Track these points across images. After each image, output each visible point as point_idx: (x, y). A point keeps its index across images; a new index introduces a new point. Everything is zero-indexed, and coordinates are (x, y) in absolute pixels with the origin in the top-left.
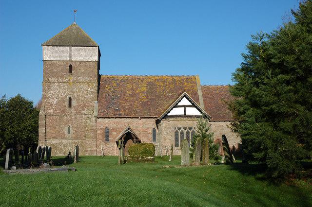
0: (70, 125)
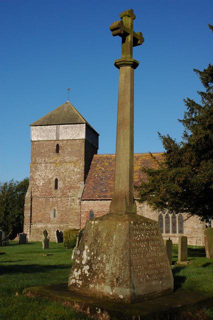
0: (56, 208)
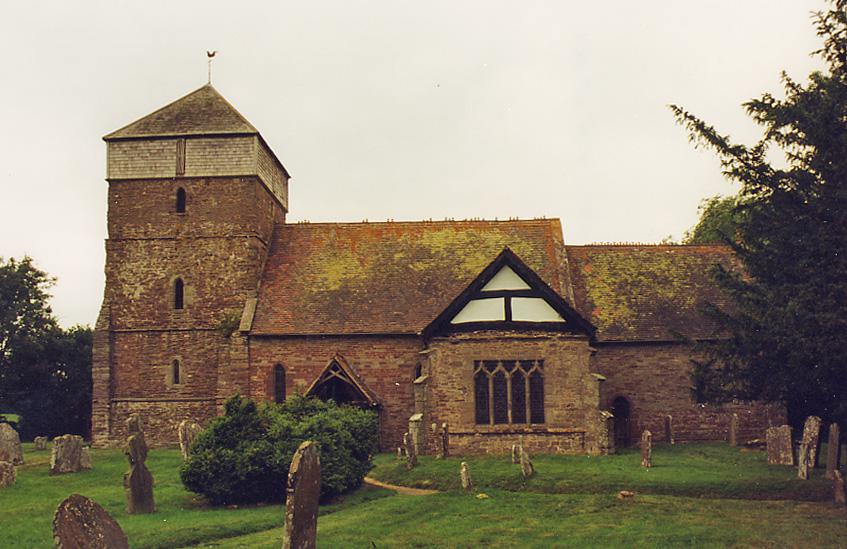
0: (179, 357)
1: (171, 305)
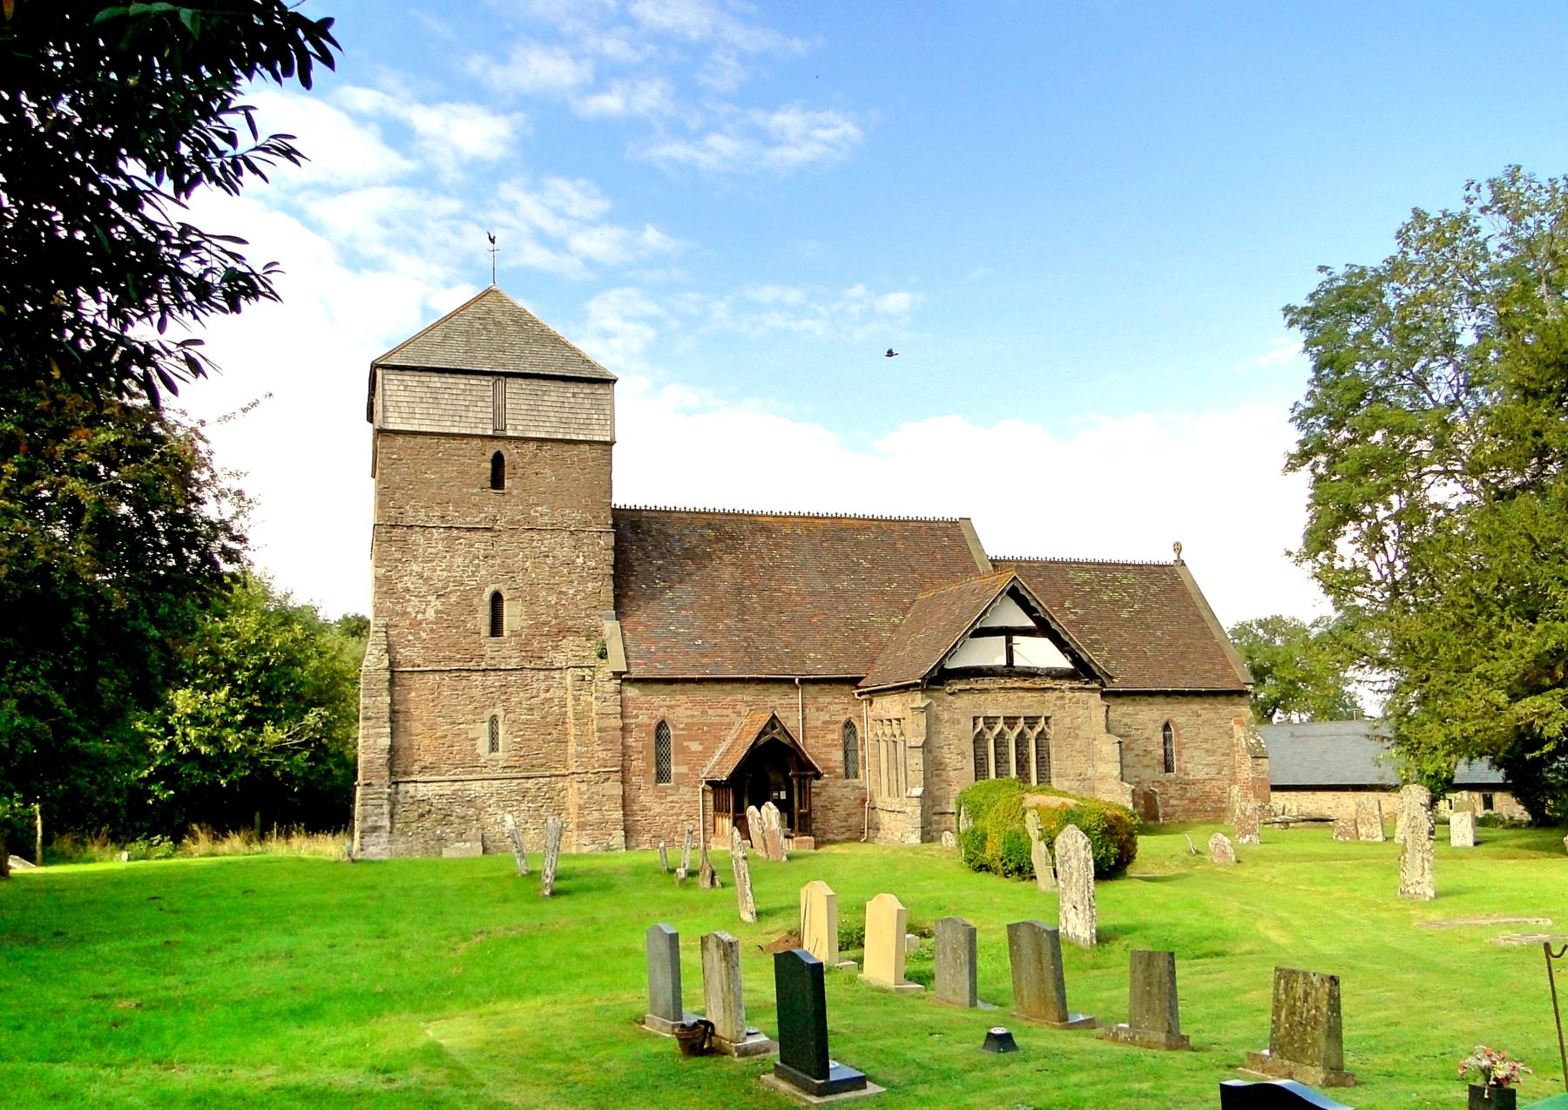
0: (499, 711)
1: (485, 630)
